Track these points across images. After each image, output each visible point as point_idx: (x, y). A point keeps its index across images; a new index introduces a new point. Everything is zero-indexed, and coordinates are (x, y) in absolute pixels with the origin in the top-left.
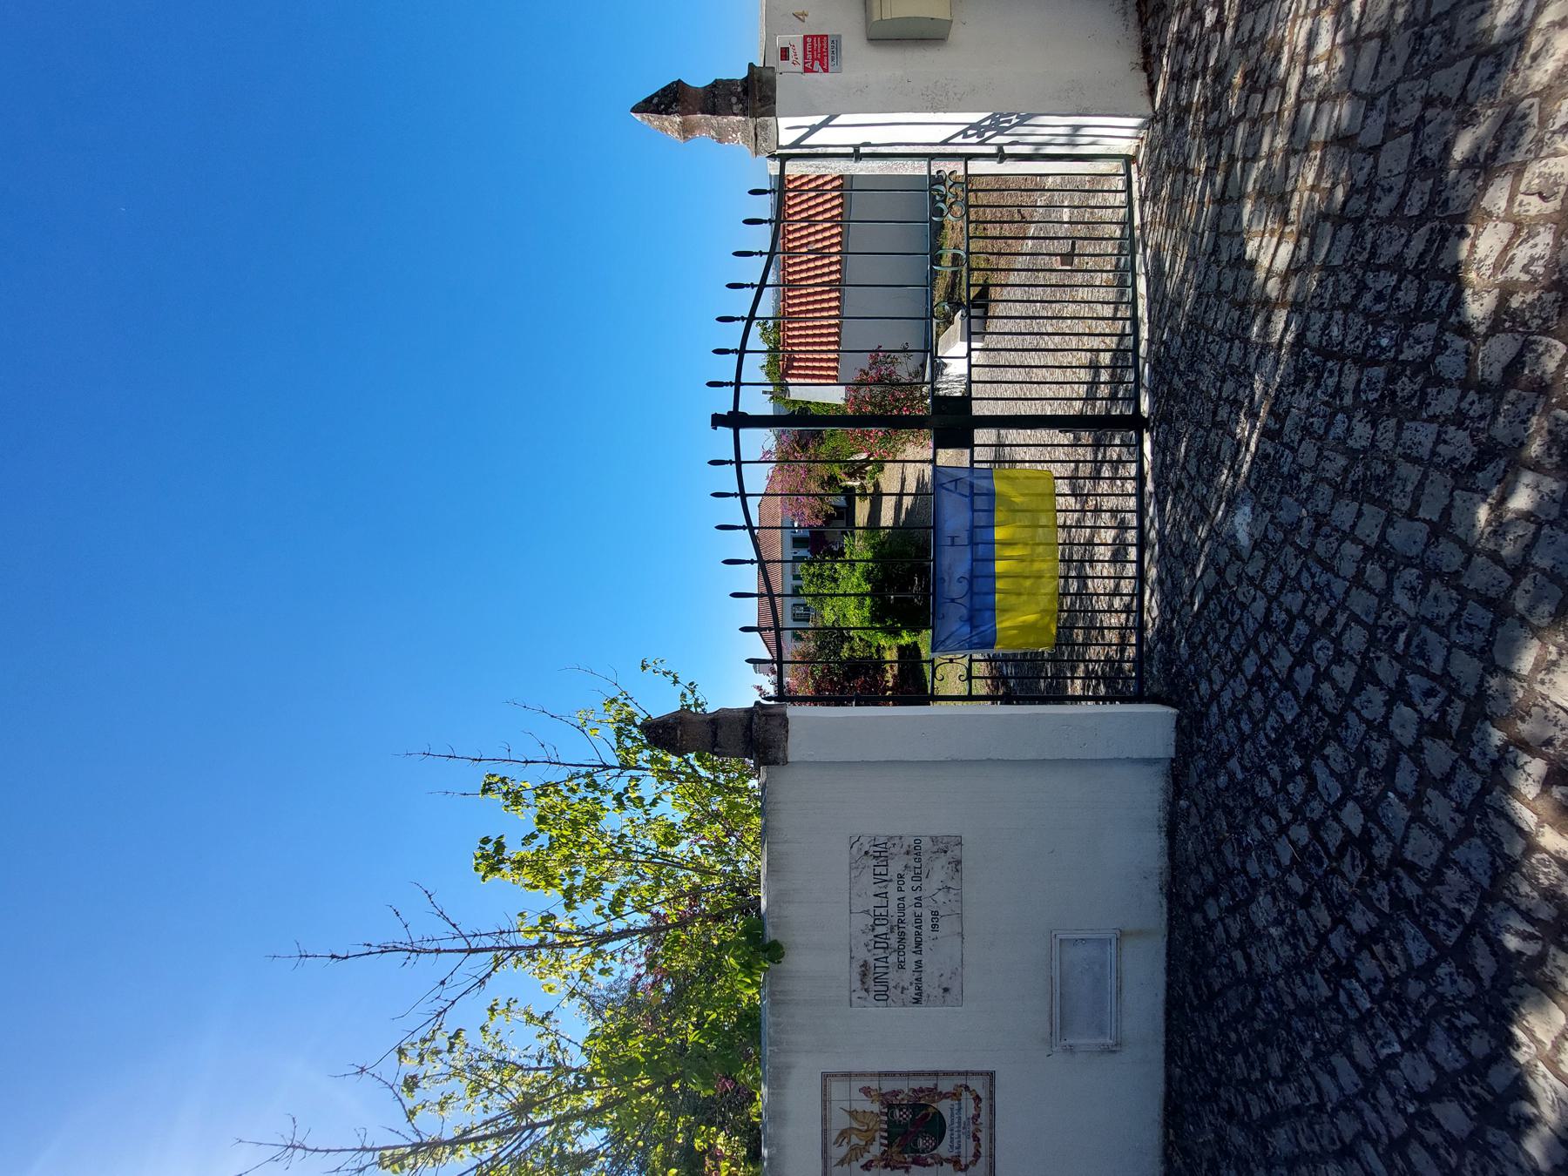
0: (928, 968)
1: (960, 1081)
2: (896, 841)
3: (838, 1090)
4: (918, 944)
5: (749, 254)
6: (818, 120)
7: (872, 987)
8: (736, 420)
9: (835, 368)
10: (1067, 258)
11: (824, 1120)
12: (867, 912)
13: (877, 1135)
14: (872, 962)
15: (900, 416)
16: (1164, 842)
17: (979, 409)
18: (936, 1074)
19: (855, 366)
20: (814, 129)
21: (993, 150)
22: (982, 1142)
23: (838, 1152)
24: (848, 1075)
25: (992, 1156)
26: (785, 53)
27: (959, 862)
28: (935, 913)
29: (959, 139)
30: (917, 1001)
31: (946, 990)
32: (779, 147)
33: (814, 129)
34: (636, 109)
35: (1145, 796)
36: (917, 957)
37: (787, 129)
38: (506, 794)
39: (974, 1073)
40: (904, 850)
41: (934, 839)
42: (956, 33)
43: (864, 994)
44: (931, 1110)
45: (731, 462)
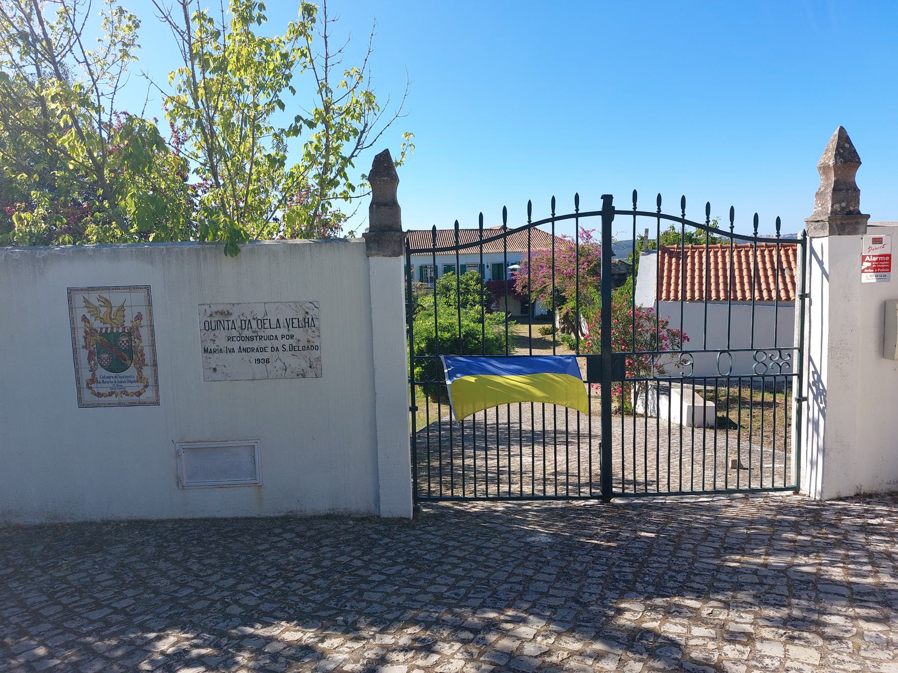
0: (230, 356)
1: (151, 382)
2: (317, 333)
3: (141, 295)
4: (246, 350)
5: (732, 219)
6: (826, 266)
7: (213, 319)
8: (608, 212)
9: (668, 298)
10: (738, 466)
11: (117, 288)
12: (266, 314)
13: (108, 326)
14: (231, 318)
15: (610, 328)
16: (322, 513)
17: (615, 385)
18: (155, 365)
19: (671, 315)
20: (821, 263)
21: (804, 394)
22: (109, 398)
23: (93, 298)
24: (150, 304)
25: (99, 405)
26: (877, 241)
27: (304, 377)
28: (267, 361)
29: (812, 369)
30: (206, 351)
31: (215, 370)
32: (811, 238)
33: (821, 263)
34: (842, 129)
35: (356, 501)
36: (236, 349)
37: (821, 244)
38: (303, 24)
39: (157, 390)
40: (311, 339)
41: (319, 359)
42: (887, 364)
43: (208, 313)
44: (129, 362)
45: (577, 210)
